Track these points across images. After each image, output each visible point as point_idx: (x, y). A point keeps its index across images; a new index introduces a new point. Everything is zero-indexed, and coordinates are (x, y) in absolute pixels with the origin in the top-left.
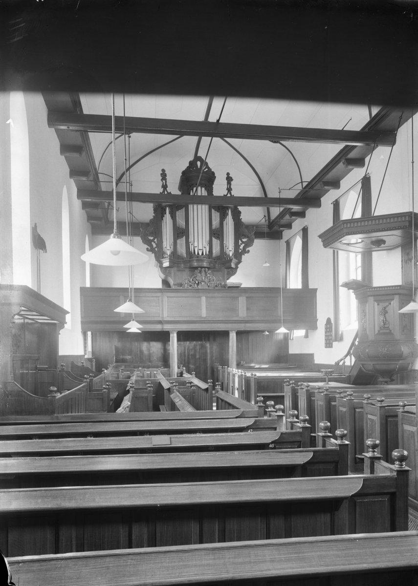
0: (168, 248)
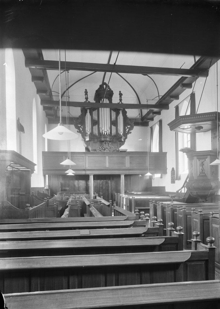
0: (89, 131)
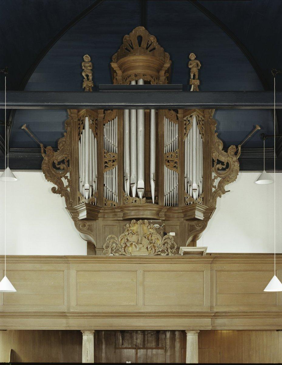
0: (87, 186)
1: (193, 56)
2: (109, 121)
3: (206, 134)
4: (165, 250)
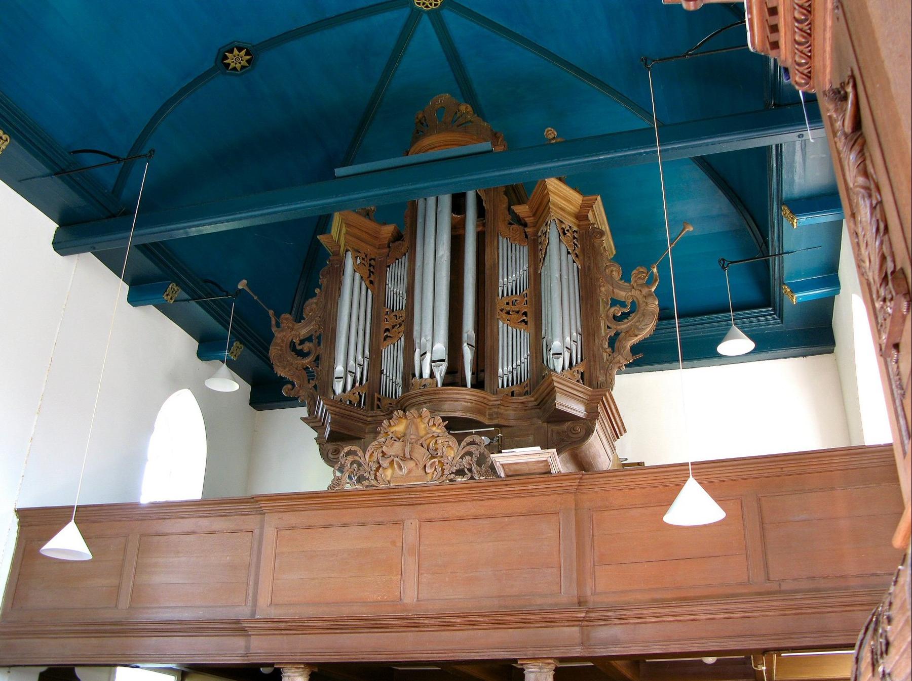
1: (550, 132)
2: (397, 259)
3: (584, 254)
4: (466, 470)
